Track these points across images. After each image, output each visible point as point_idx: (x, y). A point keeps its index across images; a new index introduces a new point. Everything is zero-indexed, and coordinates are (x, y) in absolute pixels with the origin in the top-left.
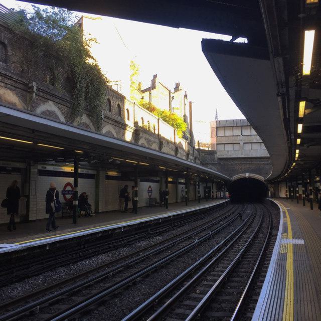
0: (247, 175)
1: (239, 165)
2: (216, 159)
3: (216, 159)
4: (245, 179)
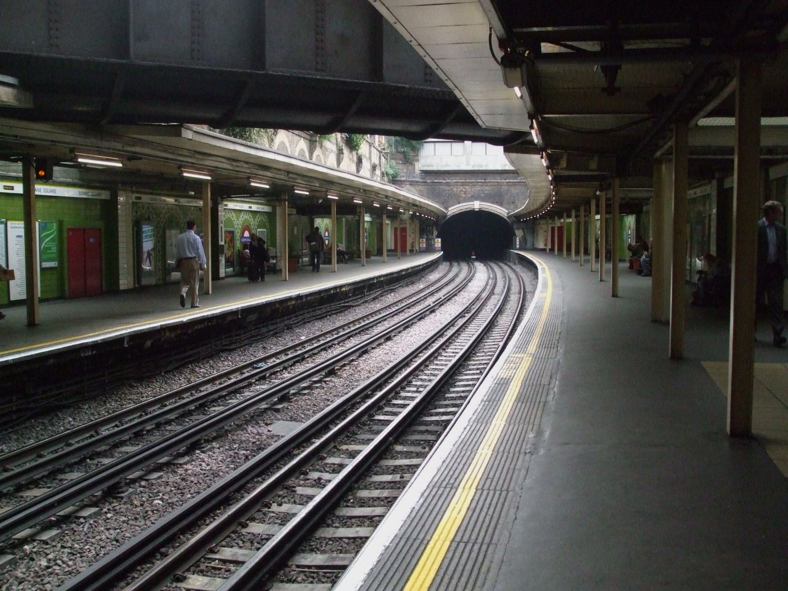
0: (477, 205)
1: (463, 184)
2: (417, 171)
3: (417, 171)
4: (471, 213)
